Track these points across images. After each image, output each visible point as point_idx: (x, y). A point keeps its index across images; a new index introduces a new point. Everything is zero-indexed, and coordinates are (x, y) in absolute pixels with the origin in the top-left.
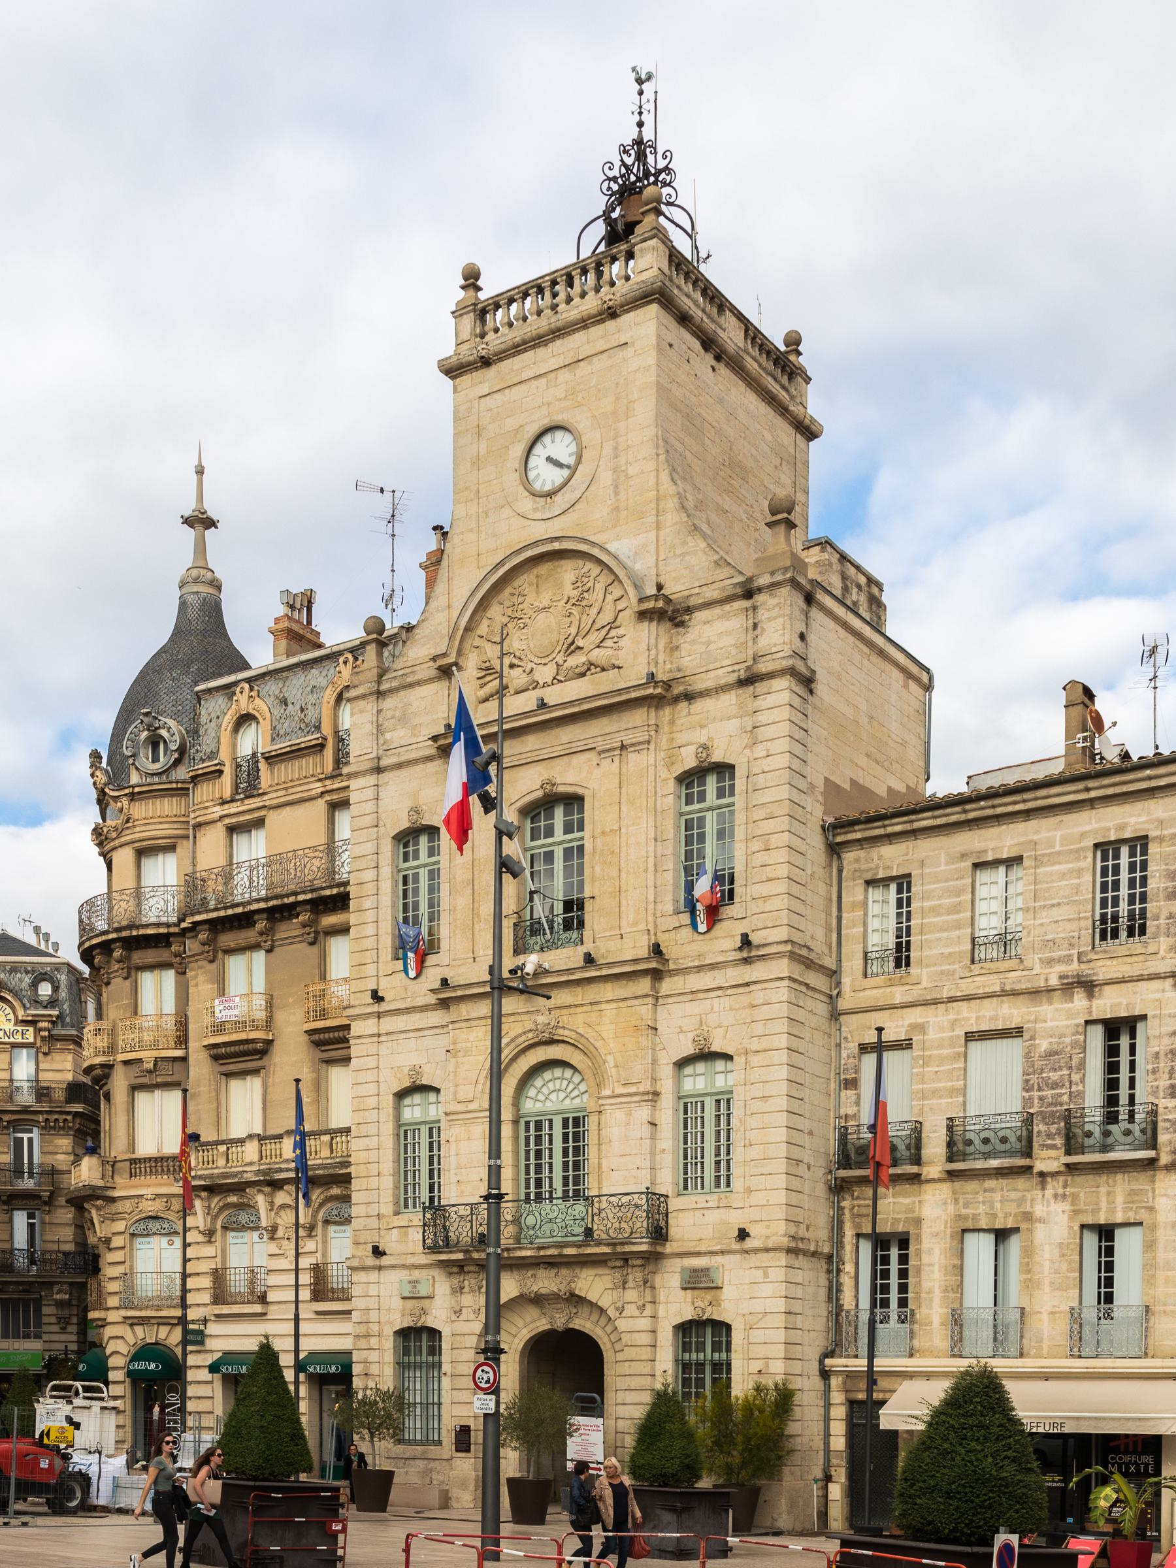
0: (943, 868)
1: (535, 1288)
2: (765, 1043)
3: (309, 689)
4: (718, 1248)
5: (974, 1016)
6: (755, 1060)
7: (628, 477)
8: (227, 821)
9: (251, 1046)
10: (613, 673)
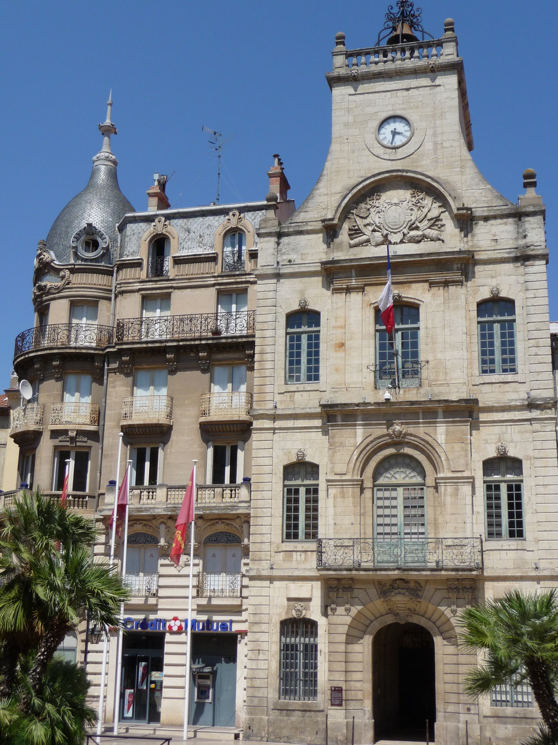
2: (542, 454)
6: (538, 463)
7: (443, 147)
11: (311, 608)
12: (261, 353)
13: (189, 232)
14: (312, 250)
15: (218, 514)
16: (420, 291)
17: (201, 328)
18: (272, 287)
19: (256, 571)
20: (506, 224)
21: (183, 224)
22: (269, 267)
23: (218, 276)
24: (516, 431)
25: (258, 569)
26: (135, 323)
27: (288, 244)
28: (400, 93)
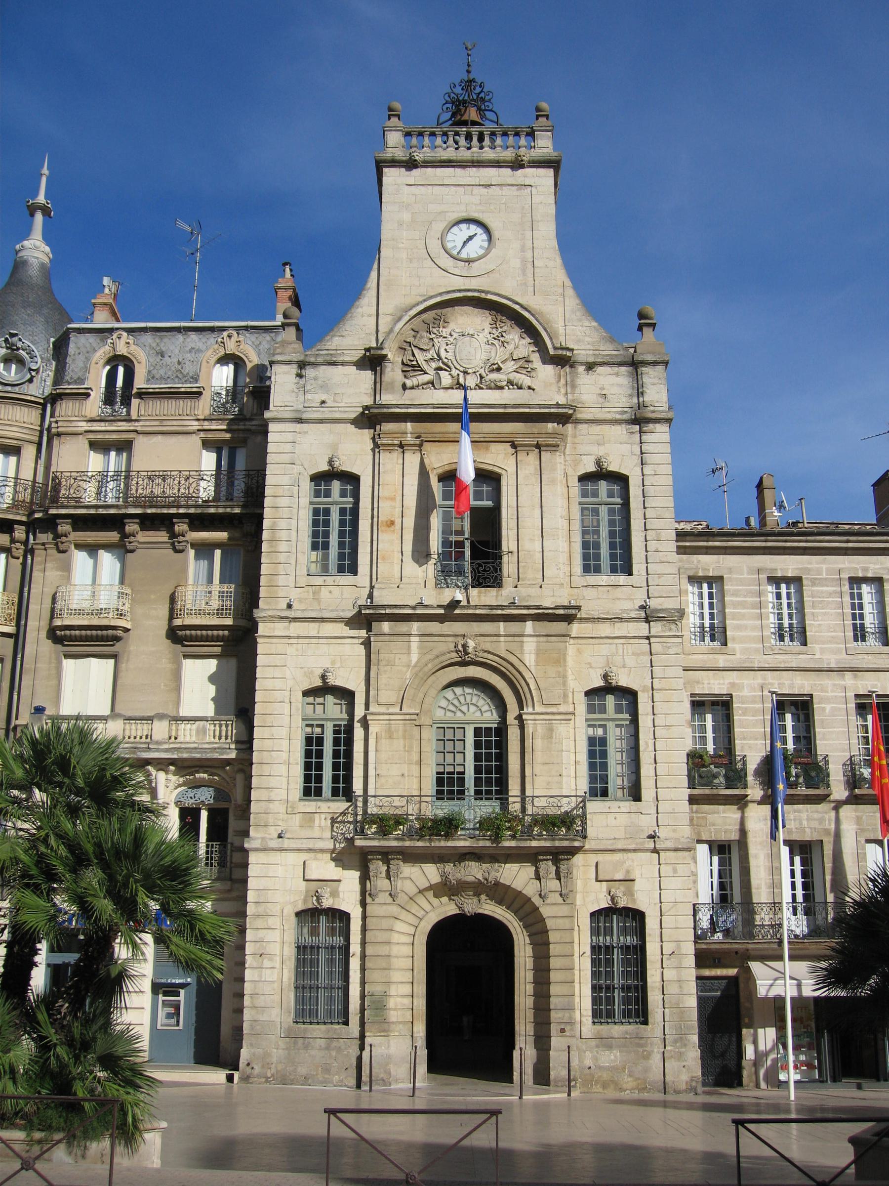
0: (745, 576)
1: (459, 876)
3: (187, 349)
4: (633, 846)
5: (776, 682)
8: (91, 436)
9: (110, 632)
10: (525, 393)
11: (341, 895)
12: (272, 529)
13: (163, 356)
14: (354, 389)
15: (199, 759)
16: (501, 456)
17: (179, 490)
18: (289, 437)
19: (259, 841)
20: (617, 374)
21: (154, 345)
22: (286, 408)
23: (204, 420)
24: (630, 652)
25: (263, 838)
26: (79, 478)
27: (315, 379)
28: (477, 190)
